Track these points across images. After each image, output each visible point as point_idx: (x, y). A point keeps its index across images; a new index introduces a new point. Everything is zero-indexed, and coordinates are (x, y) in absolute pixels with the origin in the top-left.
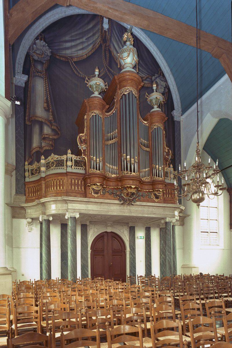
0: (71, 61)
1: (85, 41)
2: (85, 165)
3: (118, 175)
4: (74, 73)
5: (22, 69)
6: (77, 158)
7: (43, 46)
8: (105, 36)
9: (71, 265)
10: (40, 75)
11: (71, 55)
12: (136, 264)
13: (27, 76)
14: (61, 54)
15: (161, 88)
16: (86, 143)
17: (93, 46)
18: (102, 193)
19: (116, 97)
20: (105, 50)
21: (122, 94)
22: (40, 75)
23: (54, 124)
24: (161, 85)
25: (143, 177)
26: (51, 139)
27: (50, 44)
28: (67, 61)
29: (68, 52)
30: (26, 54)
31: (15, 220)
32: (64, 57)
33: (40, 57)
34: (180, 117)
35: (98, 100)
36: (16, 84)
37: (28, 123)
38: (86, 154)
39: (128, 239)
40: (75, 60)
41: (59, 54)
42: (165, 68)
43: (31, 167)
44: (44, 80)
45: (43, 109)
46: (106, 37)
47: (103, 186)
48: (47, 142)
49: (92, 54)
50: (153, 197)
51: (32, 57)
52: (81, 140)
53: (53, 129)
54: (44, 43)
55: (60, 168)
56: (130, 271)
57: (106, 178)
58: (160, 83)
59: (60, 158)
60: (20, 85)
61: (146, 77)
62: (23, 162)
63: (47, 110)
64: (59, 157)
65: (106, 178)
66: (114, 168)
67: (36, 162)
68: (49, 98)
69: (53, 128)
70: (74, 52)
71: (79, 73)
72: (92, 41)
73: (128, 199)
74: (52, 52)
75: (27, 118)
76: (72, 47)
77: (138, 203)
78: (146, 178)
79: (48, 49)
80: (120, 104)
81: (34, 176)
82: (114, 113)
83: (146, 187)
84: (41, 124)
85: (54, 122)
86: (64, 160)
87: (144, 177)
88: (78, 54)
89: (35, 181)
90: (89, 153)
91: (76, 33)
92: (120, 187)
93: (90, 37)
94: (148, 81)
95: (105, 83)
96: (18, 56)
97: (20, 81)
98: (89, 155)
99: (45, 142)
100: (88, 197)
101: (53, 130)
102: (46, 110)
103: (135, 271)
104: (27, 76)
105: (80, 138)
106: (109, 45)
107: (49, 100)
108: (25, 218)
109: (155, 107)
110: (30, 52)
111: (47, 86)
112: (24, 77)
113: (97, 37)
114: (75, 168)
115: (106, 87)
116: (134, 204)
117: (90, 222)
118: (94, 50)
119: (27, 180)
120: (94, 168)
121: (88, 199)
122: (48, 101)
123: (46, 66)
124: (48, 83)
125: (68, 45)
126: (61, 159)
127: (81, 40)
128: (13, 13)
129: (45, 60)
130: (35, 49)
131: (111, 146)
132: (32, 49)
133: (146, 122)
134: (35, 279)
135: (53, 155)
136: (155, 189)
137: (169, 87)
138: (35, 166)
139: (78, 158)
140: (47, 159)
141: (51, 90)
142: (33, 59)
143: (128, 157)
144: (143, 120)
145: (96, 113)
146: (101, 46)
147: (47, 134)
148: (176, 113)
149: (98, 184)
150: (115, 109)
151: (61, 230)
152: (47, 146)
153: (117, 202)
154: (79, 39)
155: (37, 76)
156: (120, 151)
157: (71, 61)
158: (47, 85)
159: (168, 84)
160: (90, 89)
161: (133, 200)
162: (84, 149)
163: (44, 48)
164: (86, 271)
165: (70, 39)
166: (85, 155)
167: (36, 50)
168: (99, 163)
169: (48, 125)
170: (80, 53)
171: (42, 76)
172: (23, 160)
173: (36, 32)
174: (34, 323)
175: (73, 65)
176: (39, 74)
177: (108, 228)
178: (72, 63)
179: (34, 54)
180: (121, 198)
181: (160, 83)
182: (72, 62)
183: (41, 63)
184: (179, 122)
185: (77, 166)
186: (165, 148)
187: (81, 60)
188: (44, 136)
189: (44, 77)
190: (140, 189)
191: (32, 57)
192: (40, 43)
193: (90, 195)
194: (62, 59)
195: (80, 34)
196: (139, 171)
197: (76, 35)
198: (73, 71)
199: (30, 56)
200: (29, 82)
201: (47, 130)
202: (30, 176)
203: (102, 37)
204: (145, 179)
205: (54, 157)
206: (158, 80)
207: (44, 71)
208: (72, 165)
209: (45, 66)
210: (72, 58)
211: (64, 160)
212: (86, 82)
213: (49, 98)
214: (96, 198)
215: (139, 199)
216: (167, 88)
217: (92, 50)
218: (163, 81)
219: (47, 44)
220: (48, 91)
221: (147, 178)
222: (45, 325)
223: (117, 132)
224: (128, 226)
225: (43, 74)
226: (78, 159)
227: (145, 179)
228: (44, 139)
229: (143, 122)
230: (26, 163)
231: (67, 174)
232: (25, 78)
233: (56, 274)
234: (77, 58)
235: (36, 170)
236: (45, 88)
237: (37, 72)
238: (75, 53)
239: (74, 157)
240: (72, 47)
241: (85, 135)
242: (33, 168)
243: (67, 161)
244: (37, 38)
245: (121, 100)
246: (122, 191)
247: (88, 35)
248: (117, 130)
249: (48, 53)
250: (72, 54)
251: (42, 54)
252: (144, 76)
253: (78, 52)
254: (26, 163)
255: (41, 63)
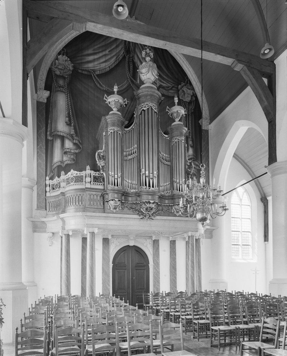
0: (94, 74)
1: (108, 53)
2: (104, 181)
3: (137, 190)
4: (97, 86)
5: (44, 85)
6: (96, 174)
7: (66, 61)
8: (129, 47)
9: (89, 280)
10: (62, 90)
11: (93, 68)
12: (159, 278)
13: (49, 92)
14: (84, 67)
15: (188, 97)
16: (104, 160)
17: (117, 58)
18: (120, 209)
19: (135, 112)
20: (129, 62)
21: (142, 110)
22: (62, 90)
23: (75, 138)
24: (188, 94)
25: (163, 192)
26: (73, 153)
27: (72, 58)
28: (89, 74)
29: (90, 65)
30: (48, 70)
31: (36, 234)
32: (86, 71)
33: (62, 72)
34: (208, 125)
35: (116, 118)
36: (38, 100)
37: (49, 138)
38: (105, 170)
39: (152, 252)
40: (98, 73)
41: (81, 68)
42: (192, 76)
43: (51, 182)
44: (66, 95)
45: (65, 124)
46: (130, 48)
47: (121, 201)
48: (68, 156)
49: (115, 66)
50: (174, 211)
51: (54, 73)
52: (99, 156)
53: (75, 143)
54: (66, 58)
55: (79, 184)
56: (154, 286)
57: (125, 193)
58: (187, 91)
59: (80, 174)
60: (41, 101)
61: (171, 86)
62: (45, 177)
63: (69, 124)
64: (78, 173)
65: (125, 193)
66: (133, 183)
67: (57, 178)
68: (71, 112)
69: (75, 142)
70: (97, 66)
71: (101, 86)
72: (116, 53)
73: (148, 213)
74: (74, 67)
75: (48, 133)
76: (94, 60)
77: (158, 217)
78: (166, 192)
79: (70, 64)
80: (140, 120)
81: (55, 190)
82: (133, 129)
83: (167, 201)
84: (63, 138)
85: (76, 136)
86: (83, 176)
87: (165, 191)
88: (101, 67)
89: (56, 196)
90: (107, 169)
91: (99, 46)
92: (139, 202)
93: (113, 49)
94: (173, 90)
95: (124, 99)
96: (41, 73)
97: (42, 97)
98: (107, 170)
99: (66, 156)
100: (107, 212)
101: (75, 144)
102: (68, 124)
103: (159, 286)
104: (49, 92)
105: (99, 155)
106: (133, 56)
107: (71, 114)
108: (45, 232)
109: (177, 120)
110: (53, 67)
111: (69, 101)
112: (46, 93)
113: (120, 49)
114: (93, 184)
115: (125, 103)
116: (154, 218)
117: (112, 236)
118: (117, 62)
119: (48, 194)
120: (112, 184)
121: (107, 214)
122: (70, 115)
123: (68, 80)
124: (70, 97)
125: (91, 58)
126: (80, 175)
127: (104, 53)
128: (30, 45)
129: (67, 75)
130: (57, 64)
131: (135, 159)
132: (54, 64)
133: (167, 136)
134: (235, 291)
135: (72, 171)
136: (175, 203)
137: (196, 95)
138: (56, 180)
139: (97, 174)
140: (67, 175)
141: (72, 103)
142: (55, 74)
143: (147, 172)
144: (163, 134)
145: (114, 130)
146: (124, 57)
147: (69, 149)
148: (204, 123)
149: (116, 200)
150: (134, 125)
151: (82, 244)
152: (69, 160)
153: (137, 216)
154: (102, 51)
155: (58, 91)
156: (139, 166)
157: (94, 74)
158: (69, 99)
159: (195, 92)
160: (109, 105)
161: (152, 214)
162: (102, 165)
163: (67, 63)
164: (107, 286)
165: (92, 52)
166: (103, 171)
167: (58, 66)
168: (117, 178)
169: (70, 140)
170: (103, 65)
171: (64, 91)
172: (45, 174)
173: (58, 48)
174: (76, 347)
175: (96, 78)
176: (61, 88)
177: (130, 241)
178: (95, 77)
179: (56, 69)
180: (140, 213)
181: (187, 91)
182: (95, 75)
183: (63, 77)
184: (207, 131)
185: (96, 182)
186: (187, 161)
187: (103, 72)
188: (65, 151)
189: (66, 91)
190: (160, 204)
191: (54, 73)
192: (63, 58)
193: (108, 211)
194: (84, 72)
195: (102, 46)
196: (158, 185)
197: (99, 48)
198: (95, 84)
199: (52, 72)
200: (51, 97)
201: (68, 144)
202: (51, 191)
203: (125, 48)
204: (165, 193)
205: (73, 173)
206: (185, 89)
207: (66, 86)
208: (91, 181)
209: (67, 80)
210: (94, 71)
211: (83, 176)
212: (104, 99)
213: (71, 112)
214: (115, 213)
215: (159, 213)
216: (195, 97)
217: (116, 62)
218: (190, 89)
219: (69, 58)
220: (69, 105)
221: (168, 192)
222: (91, 350)
223: (136, 147)
224: (152, 239)
225: (65, 89)
226: (97, 175)
227: (165, 193)
228: (66, 153)
229: (164, 136)
230: (47, 178)
231: (87, 189)
232: (47, 94)
233: (76, 290)
234: (100, 71)
235: (57, 185)
236: (66, 102)
237: (60, 87)
238: (98, 66)
239: (93, 173)
240: (94, 60)
241: (104, 151)
242: (54, 183)
243: (86, 177)
244: (59, 54)
245: (141, 115)
246: (141, 206)
247: (111, 47)
248: (136, 145)
249: (70, 68)
250: (94, 67)
251: (65, 69)
252: (170, 85)
253: (101, 65)
254: (47, 178)
255: (63, 77)
